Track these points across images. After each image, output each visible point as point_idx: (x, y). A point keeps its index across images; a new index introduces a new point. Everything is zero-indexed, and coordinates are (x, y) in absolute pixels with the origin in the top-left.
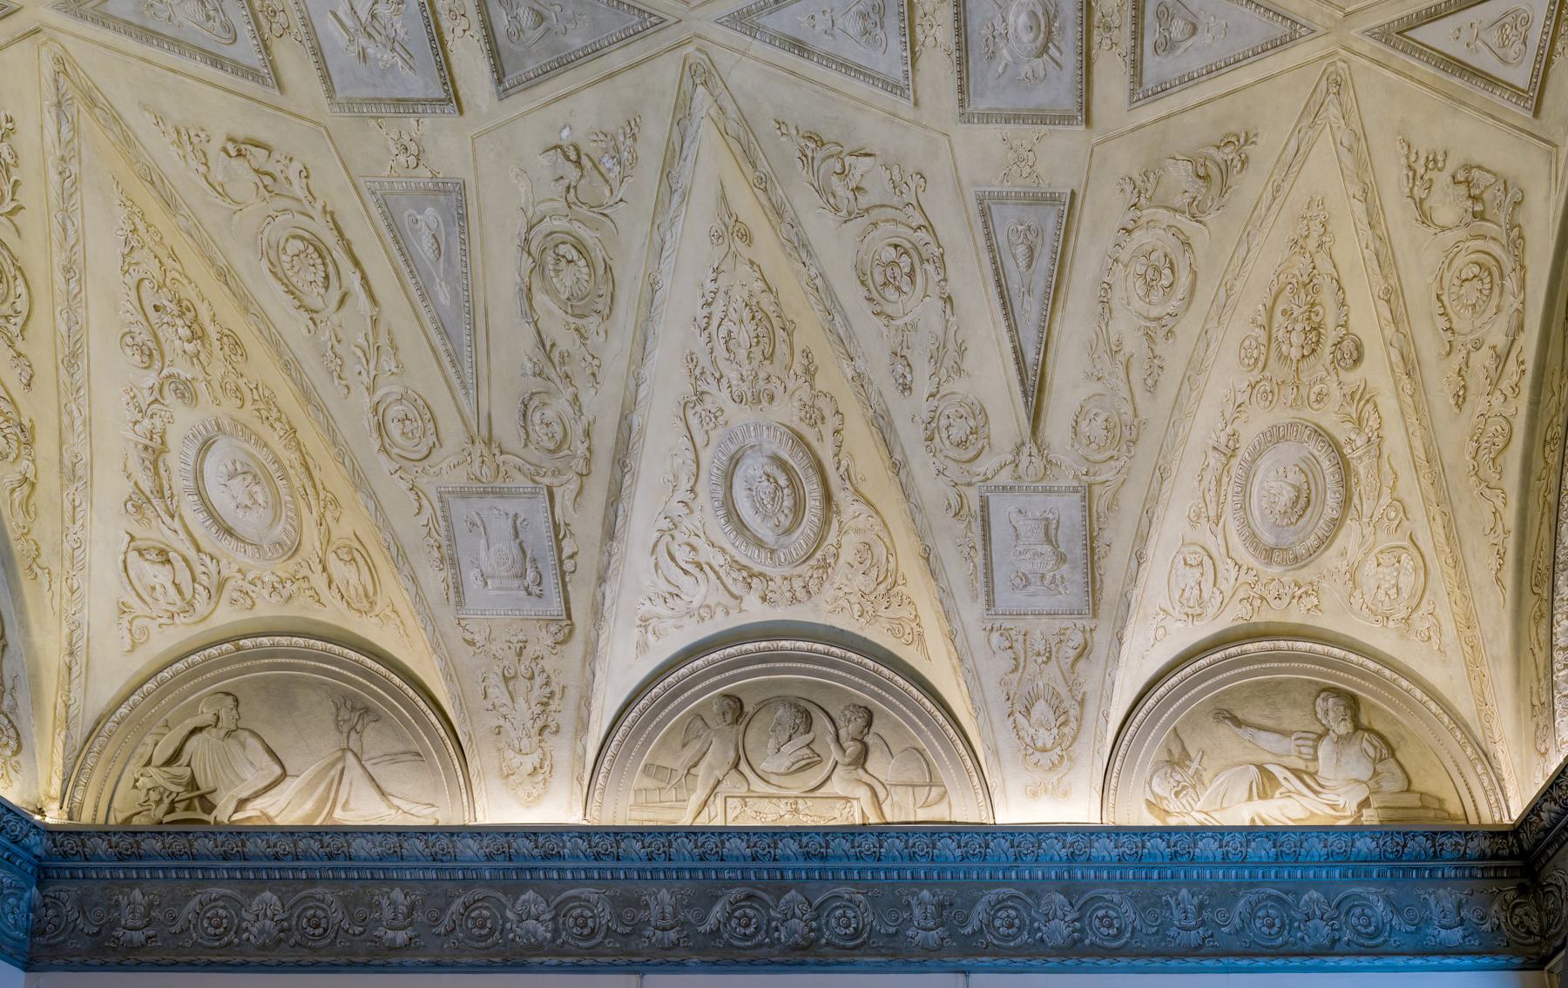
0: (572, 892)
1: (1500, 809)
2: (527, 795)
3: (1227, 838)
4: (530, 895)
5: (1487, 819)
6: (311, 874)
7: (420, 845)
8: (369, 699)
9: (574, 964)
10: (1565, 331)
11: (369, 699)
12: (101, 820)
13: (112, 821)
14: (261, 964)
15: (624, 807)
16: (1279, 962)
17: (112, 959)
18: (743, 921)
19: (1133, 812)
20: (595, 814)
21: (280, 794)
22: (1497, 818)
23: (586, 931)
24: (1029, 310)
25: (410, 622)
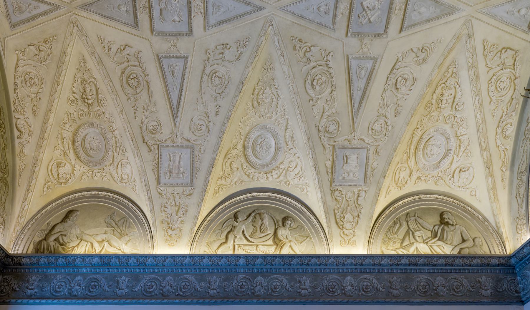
0: (275, 276)
1: (502, 250)
2: (357, 245)
3: (231, 258)
4: (349, 278)
5: (498, 253)
6: (468, 271)
7: (316, 261)
8: (119, 210)
9: (317, 302)
10: (526, 98)
11: (119, 210)
12: (24, 252)
13: (102, 253)
14: (461, 302)
15: (201, 249)
16: (44, 301)
17: (273, 301)
18: (185, 286)
19: (376, 250)
20: (194, 250)
21: (91, 242)
22: (502, 253)
23: (148, 290)
24: (359, 85)
25: (499, 184)
